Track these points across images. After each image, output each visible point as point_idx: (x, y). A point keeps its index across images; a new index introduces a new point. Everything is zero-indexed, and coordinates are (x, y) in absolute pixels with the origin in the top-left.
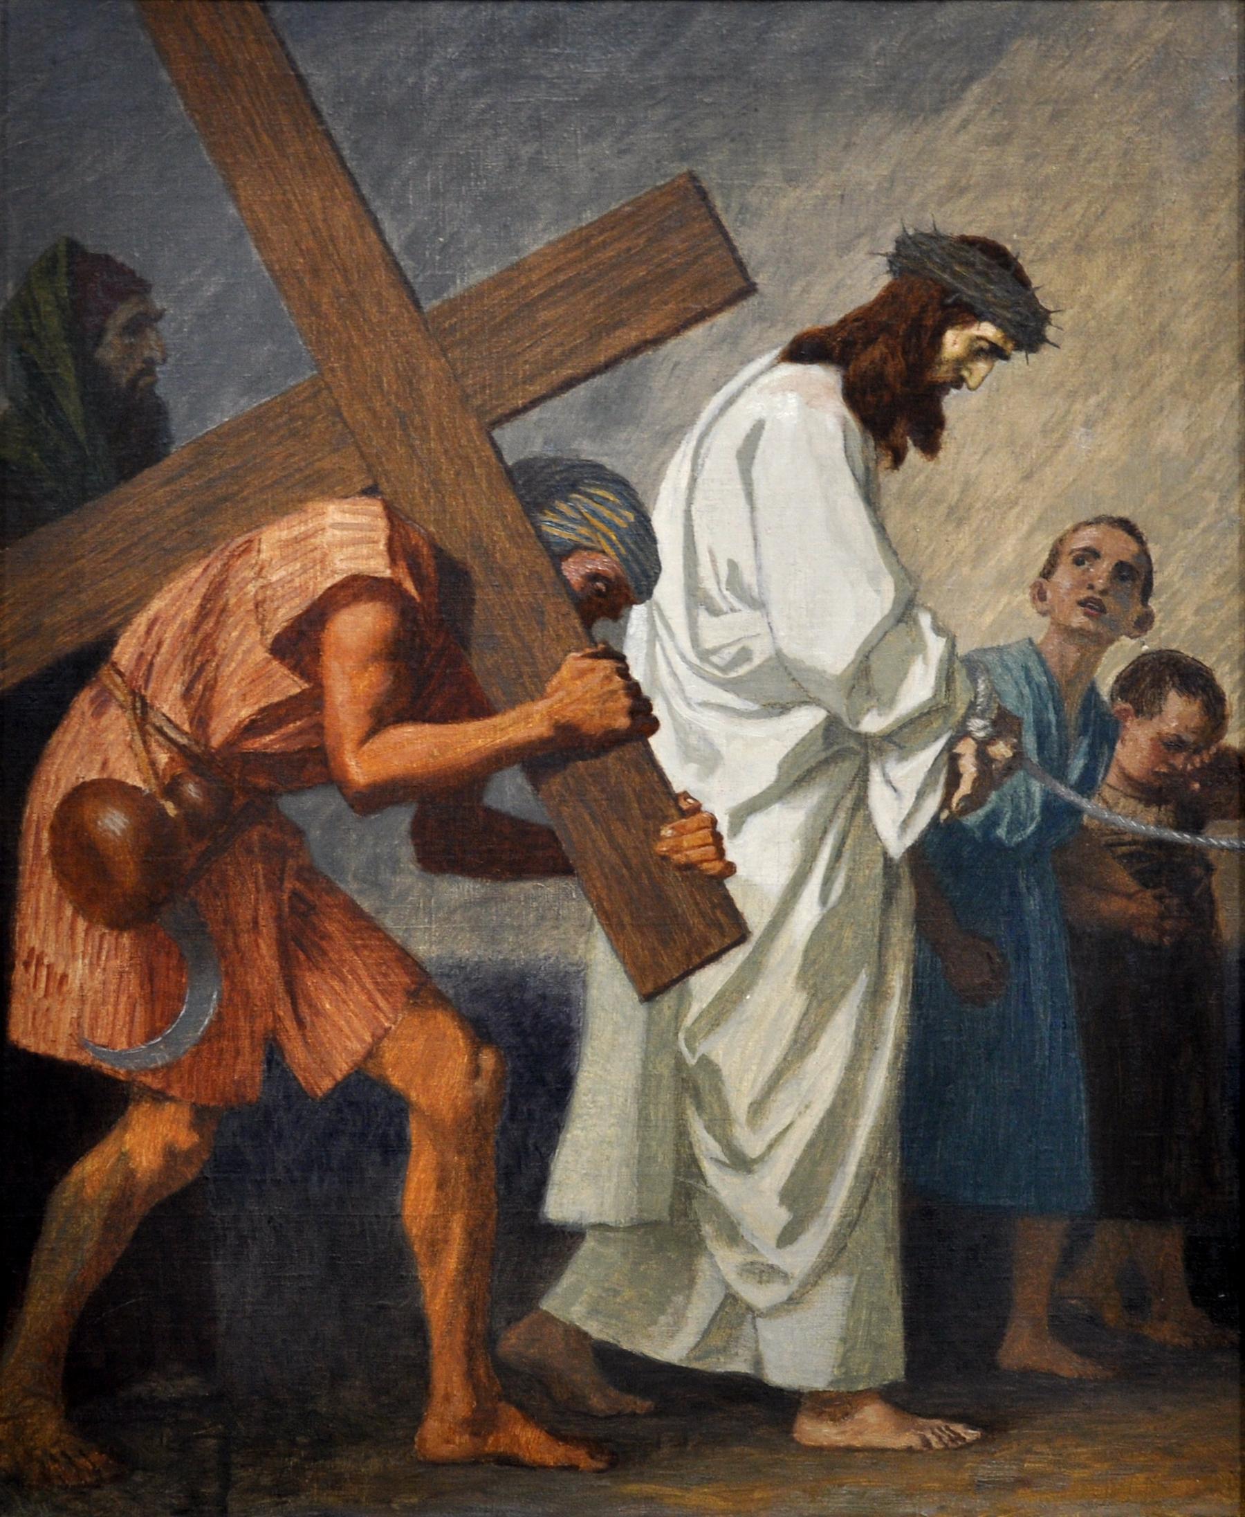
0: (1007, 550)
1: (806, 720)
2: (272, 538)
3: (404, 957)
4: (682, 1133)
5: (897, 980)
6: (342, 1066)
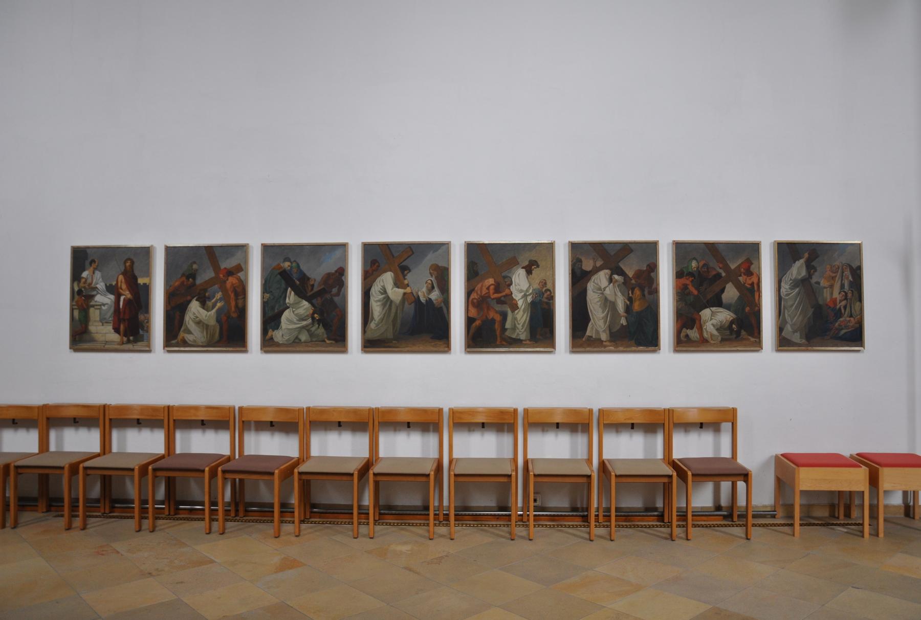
0: (537, 282)
1: (523, 294)
2: (486, 281)
3: (495, 310)
4: (514, 322)
5: (529, 312)
6: (491, 317)
